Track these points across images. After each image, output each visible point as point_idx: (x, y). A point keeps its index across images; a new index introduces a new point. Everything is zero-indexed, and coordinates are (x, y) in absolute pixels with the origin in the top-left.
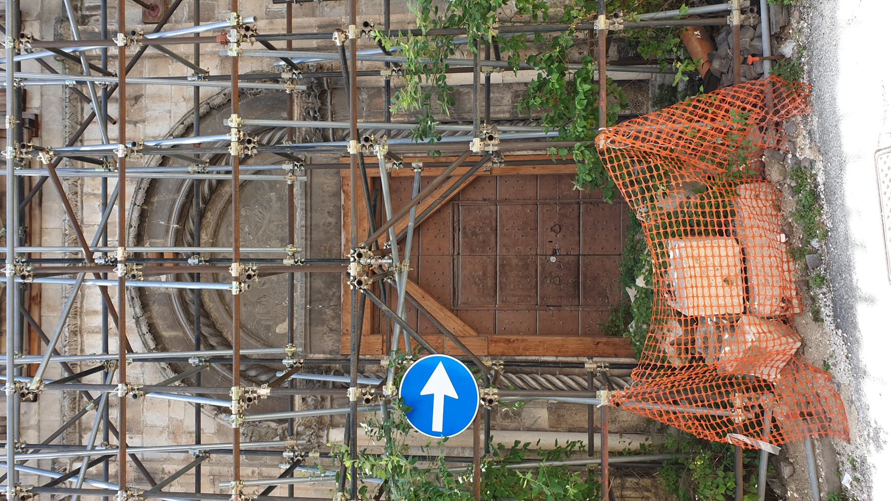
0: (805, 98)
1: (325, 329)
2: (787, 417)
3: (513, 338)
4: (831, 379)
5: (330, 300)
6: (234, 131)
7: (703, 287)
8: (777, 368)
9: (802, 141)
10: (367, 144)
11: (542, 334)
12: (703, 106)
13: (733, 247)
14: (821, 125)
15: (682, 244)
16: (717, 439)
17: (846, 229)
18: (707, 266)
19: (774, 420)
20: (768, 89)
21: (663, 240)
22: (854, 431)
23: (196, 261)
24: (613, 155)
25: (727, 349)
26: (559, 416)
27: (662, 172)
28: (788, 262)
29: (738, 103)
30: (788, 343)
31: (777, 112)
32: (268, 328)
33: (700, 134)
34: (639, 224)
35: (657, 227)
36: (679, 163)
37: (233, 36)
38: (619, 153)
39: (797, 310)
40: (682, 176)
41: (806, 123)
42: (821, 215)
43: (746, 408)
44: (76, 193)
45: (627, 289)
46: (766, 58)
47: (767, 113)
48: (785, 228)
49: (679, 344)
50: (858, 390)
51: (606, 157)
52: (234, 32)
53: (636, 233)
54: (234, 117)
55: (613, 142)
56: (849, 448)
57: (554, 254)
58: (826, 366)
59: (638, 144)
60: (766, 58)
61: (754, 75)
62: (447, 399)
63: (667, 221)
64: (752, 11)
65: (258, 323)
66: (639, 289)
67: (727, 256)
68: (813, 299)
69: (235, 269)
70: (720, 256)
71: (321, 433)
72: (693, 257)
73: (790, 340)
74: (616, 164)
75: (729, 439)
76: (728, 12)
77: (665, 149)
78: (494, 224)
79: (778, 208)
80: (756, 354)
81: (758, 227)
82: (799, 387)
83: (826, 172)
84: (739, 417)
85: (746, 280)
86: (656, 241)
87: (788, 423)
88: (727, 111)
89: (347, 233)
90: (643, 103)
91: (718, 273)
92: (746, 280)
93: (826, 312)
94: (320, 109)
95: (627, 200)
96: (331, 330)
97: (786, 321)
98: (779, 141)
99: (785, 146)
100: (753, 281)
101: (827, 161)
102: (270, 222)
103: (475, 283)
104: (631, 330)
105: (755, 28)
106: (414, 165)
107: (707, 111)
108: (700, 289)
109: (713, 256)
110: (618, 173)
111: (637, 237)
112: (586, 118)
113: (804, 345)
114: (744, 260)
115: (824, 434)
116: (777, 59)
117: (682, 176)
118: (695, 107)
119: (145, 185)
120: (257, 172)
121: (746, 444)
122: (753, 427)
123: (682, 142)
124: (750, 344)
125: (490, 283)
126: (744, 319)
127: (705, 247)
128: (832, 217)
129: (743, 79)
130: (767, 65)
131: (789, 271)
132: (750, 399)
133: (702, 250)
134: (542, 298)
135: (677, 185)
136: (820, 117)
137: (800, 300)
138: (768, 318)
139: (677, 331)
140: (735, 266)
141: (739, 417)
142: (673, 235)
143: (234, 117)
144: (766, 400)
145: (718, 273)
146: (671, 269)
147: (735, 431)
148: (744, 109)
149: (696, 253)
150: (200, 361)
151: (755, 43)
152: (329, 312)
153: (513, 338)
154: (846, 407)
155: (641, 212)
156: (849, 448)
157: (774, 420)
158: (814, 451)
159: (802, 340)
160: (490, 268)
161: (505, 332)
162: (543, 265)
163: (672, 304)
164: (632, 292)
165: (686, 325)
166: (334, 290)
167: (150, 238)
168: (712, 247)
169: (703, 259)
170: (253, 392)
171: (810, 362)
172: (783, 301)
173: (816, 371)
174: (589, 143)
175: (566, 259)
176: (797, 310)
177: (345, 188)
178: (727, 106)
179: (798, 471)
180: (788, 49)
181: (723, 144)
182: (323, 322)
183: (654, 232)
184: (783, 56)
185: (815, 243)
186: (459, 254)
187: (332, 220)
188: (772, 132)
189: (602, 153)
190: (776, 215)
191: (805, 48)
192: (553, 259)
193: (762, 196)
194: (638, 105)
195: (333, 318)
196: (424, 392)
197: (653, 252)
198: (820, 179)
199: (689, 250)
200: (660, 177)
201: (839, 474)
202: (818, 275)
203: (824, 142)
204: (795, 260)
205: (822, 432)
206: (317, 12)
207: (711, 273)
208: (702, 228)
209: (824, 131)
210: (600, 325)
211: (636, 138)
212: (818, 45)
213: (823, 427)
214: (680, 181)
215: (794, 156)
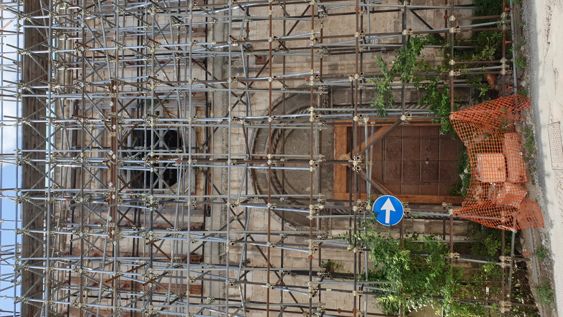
0: (529, 103)
1: (327, 190)
2: (522, 220)
3: (409, 196)
4: (538, 205)
5: (329, 178)
6: (312, 113)
7: (490, 171)
8: (519, 202)
9: (528, 118)
10: (361, 117)
11: (422, 194)
12: (490, 105)
13: (501, 156)
14: (534, 113)
15: (482, 156)
16: (494, 227)
17: (542, 150)
18: (491, 164)
19: (517, 221)
20: (516, 98)
21: (475, 154)
22: (545, 223)
23: (284, 160)
24: (456, 122)
25: (499, 195)
26: (429, 228)
27: (475, 129)
28: (523, 163)
29: (504, 104)
30: (522, 192)
31: (518, 108)
32: (303, 189)
33: (489, 115)
34: (466, 148)
35: (473, 149)
36: (481, 125)
37: (312, 78)
38: (458, 121)
39: (526, 181)
40: (482, 131)
41: (529, 112)
42: (534, 145)
43: (506, 217)
44: (228, 133)
45: (460, 175)
46: (515, 87)
47: (515, 108)
48: (522, 150)
49: (480, 196)
50: (546, 208)
51: (454, 123)
52: (312, 77)
53: (464, 151)
54: (312, 108)
55: (456, 117)
56: (544, 230)
57: (428, 160)
58: (537, 201)
59: (466, 118)
60: (515, 87)
61: (511, 93)
62: (391, 211)
63: (476, 147)
64: (510, 69)
65: (299, 186)
66: (465, 174)
67: (499, 160)
68: (532, 176)
69: (311, 162)
70: (496, 160)
71: (328, 231)
72: (486, 160)
73: (523, 191)
74: (457, 125)
75: (499, 227)
76: (501, 69)
77: (476, 120)
78: (400, 147)
79: (520, 142)
80: (510, 197)
81: (511, 149)
82: (527, 209)
83: (536, 130)
84: (503, 220)
85: (507, 169)
86: (472, 154)
87: (522, 222)
88: (499, 107)
89: (336, 150)
90: (467, 97)
91: (496, 166)
92: (507, 169)
93: (536, 180)
94: (328, 99)
95: (461, 139)
96: (329, 190)
97: (522, 185)
98: (520, 118)
99: (522, 119)
100: (509, 169)
101: (536, 126)
102: (304, 145)
103: (392, 172)
104: (461, 190)
105: (511, 75)
106: (371, 123)
107: (492, 107)
108: (488, 172)
109: (494, 160)
110: (458, 129)
111: (465, 153)
112: (445, 108)
113: (528, 193)
114: (506, 162)
115: (535, 227)
116: (519, 87)
117: (482, 131)
118: (487, 105)
119: (257, 130)
120: (298, 126)
121: (505, 229)
122: (509, 223)
123: (482, 118)
124: (507, 193)
125: (398, 172)
126: (506, 183)
127: (491, 156)
128: (538, 146)
129: (506, 94)
130: (515, 90)
131: (524, 166)
132: (508, 213)
133: (490, 158)
134: (422, 179)
135: (480, 133)
136: (534, 110)
137: (527, 177)
138: (515, 184)
139: (479, 190)
140: (502, 164)
141: (503, 220)
142: (479, 152)
143: (312, 108)
144: (514, 214)
145: (496, 166)
146: (478, 166)
147: (501, 224)
148: (506, 106)
149: (487, 159)
150: (285, 199)
151: (511, 81)
152: (329, 183)
153: (409, 196)
154: (543, 215)
155: (466, 143)
156: (544, 230)
157: (517, 221)
158: (532, 233)
159: (528, 192)
160: (398, 166)
161: (405, 193)
162: (422, 165)
163: (478, 178)
164: (462, 176)
165: (483, 185)
166: (331, 174)
167: (257, 151)
168: (493, 156)
169: (490, 161)
170: (317, 207)
171: (531, 199)
172: (520, 177)
173: (533, 203)
174: (447, 118)
175: (433, 162)
176: (526, 181)
177: (336, 131)
178: (499, 105)
179: (526, 241)
180: (523, 84)
181: (498, 119)
182: (326, 187)
183: (472, 151)
184: (521, 86)
185: (532, 156)
186: (384, 160)
187: (330, 145)
188: (517, 114)
189: (452, 122)
190: (519, 145)
191: (529, 85)
192: (427, 162)
193: (514, 138)
194: (465, 98)
195: (330, 186)
196: (382, 209)
197: (471, 158)
198: (534, 132)
199: (485, 157)
200: (474, 131)
201: (541, 241)
202: (534, 167)
203: (535, 119)
204: (526, 162)
205: (535, 225)
206: (328, 59)
207: (493, 166)
208: (490, 150)
209: (535, 116)
210: (447, 191)
211: (465, 116)
212: (533, 84)
213: (535, 223)
214: (481, 132)
215: (525, 123)
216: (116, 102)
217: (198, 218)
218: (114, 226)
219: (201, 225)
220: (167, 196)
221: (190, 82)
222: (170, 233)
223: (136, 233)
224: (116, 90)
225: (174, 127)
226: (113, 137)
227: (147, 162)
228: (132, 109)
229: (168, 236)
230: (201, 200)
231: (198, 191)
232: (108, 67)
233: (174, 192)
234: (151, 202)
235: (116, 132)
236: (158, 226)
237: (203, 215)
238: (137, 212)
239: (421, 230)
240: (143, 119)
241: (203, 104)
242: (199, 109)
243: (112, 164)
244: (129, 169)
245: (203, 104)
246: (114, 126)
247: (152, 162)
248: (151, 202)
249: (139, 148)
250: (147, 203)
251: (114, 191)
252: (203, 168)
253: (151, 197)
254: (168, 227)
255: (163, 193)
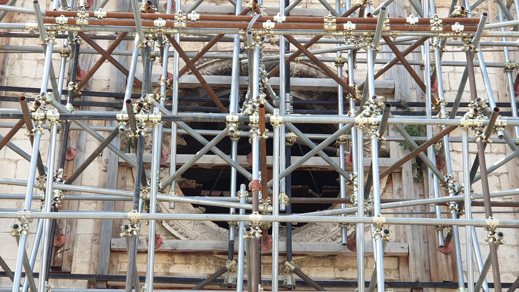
216: (418, 30)
217: (87, 259)
218: (78, 21)
219: (65, 267)
220: (154, 173)
221: (489, 222)
222: (50, 174)
223: (55, 85)
224: (450, 30)
225: (349, 192)
226: (323, 22)
227: (254, 107)
228: (393, 91)
229: (41, 169)
230: (140, 268)
231: (164, 259)
232: (502, 23)
233: (165, 187)
234: (141, 116)
235: (337, 30)
236: (70, 152)
237: (92, 273)
238: (112, 100)
239: (165, 234)
240: (374, 98)
241: (419, 275)
242: (402, 263)
243: (249, 20)
244: (233, 80)
245: (419, 275)
246: (353, 26)
247: (255, 118)
248: (141, 116)
249: (288, 105)
250: (141, 105)
251: (176, 24)
252: (234, 271)
253: (156, 116)
254: (65, 172)
255: (164, 166)
